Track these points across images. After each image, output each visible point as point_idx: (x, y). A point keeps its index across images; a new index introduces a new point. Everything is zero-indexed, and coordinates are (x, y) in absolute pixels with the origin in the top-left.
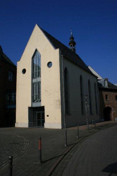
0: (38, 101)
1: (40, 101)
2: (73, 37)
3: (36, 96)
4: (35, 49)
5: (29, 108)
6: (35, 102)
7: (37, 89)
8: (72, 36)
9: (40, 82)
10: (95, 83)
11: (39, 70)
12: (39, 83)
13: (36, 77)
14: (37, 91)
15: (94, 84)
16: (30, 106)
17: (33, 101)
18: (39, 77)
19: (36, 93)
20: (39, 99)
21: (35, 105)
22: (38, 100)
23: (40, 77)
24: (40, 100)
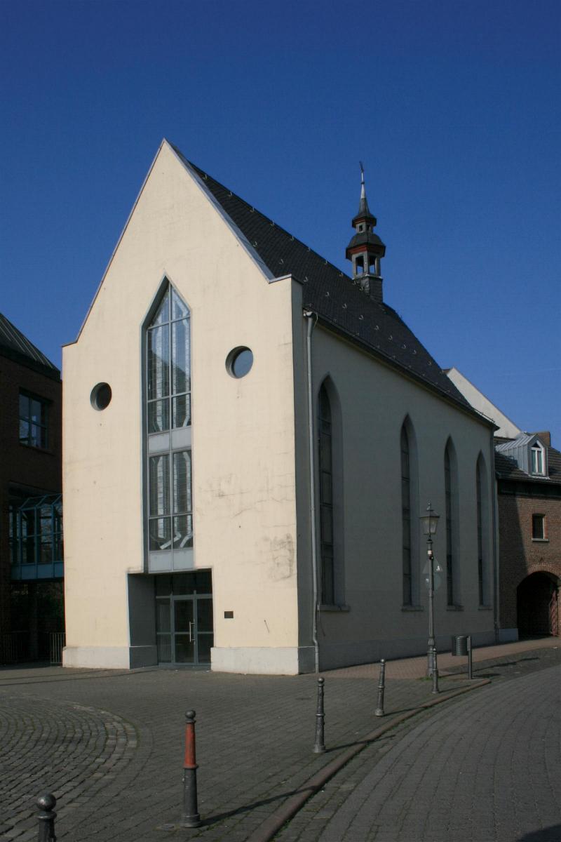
1: (190, 544)
4: (477, 453)
5: (133, 578)
7: (173, 483)
9: (189, 452)
10: (480, 455)
12: (183, 457)
14: (174, 494)
16: (138, 567)
17: (152, 543)
18: (180, 425)
19: (167, 510)
20: (184, 533)
21: (164, 563)
22: (176, 539)
23: (189, 423)
24: (187, 538)
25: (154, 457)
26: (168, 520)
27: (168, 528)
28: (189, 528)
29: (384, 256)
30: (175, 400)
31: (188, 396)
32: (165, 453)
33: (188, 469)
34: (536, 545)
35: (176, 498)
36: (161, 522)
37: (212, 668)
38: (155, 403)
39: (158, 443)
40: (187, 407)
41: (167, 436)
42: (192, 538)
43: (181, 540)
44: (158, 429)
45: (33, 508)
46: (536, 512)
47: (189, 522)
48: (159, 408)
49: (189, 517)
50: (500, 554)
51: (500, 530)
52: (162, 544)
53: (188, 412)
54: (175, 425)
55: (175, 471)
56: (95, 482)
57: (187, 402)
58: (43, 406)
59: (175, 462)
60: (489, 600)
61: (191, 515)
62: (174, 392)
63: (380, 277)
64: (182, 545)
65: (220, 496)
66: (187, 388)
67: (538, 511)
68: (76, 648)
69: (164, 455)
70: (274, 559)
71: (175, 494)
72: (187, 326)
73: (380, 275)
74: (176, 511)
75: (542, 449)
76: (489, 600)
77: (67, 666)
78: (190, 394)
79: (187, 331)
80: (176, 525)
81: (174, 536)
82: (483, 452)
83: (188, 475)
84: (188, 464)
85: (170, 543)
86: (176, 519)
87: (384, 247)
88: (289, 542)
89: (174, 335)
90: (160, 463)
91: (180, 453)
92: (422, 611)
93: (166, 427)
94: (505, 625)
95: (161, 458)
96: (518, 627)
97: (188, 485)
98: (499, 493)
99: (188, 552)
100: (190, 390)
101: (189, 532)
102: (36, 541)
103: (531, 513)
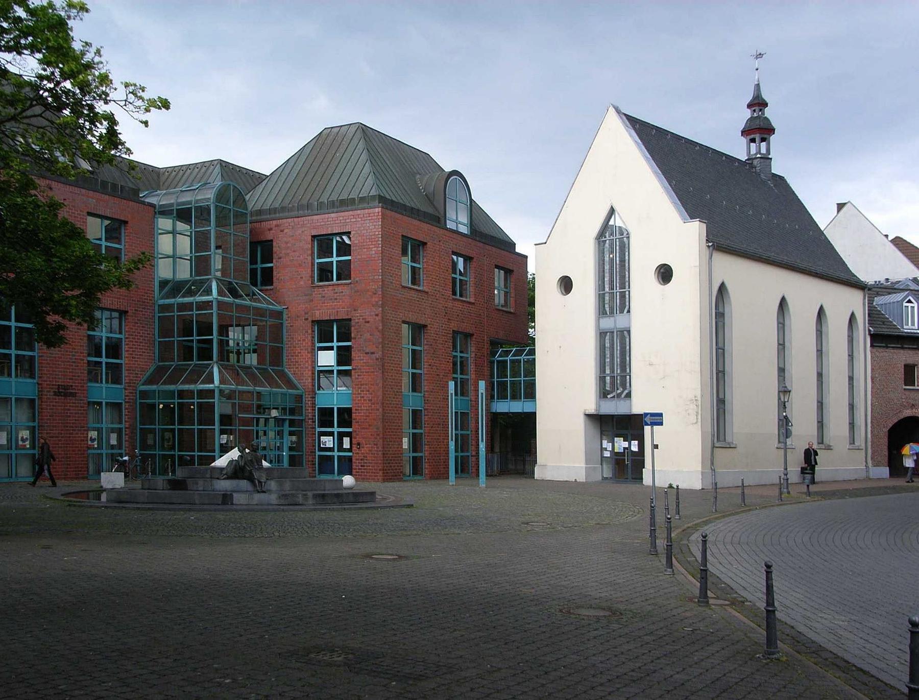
0: (619, 396)
1: (629, 395)
2: (765, 96)
3: (613, 378)
4: (851, 311)
5: (589, 416)
6: (609, 396)
7: (617, 353)
8: (758, 81)
9: (629, 332)
10: (852, 317)
11: (623, 286)
12: (624, 335)
13: (612, 312)
14: (617, 360)
15: (778, 302)
16: (592, 409)
17: (603, 394)
18: (622, 312)
19: (612, 370)
20: (624, 388)
21: (612, 407)
22: (619, 391)
23: (629, 311)
24: (626, 391)
25: (603, 333)
26: (613, 378)
27: (613, 383)
28: (628, 384)
29: (774, 134)
30: (618, 293)
31: (627, 293)
32: (612, 331)
33: (628, 343)
34: (907, 393)
35: (619, 363)
36: (608, 378)
37: (644, 483)
38: (604, 294)
39: (608, 323)
40: (627, 300)
41: (612, 319)
42: (630, 391)
43: (622, 392)
44: (607, 314)
45: (506, 358)
46: (907, 363)
47: (628, 380)
48: (607, 298)
49: (628, 377)
50: (872, 400)
51: (872, 379)
52: (608, 394)
53: (627, 304)
54: (618, 312)
55: (618, 344)
56: (560, 347)
57: (627, 296)
58: (505, 273)
59: (618, 337)
60: (860, 441)
61: (630, 376)
62: (618, 288)
63: (770, 157)
64: (623, 396)
65: (650, 365)
66: (627, 287)
67: (910, 361)
68: (546, 465)
69: (610, 332)
70: (686, 411)
71: (618, 360)
72: (627, 243)
73: (769, 154)
74: (619, 372)
75: (915, 305)
76: (860, 441)
77: (549, 477)
78: (629, 291)
79: (627, 246)
80: (618, 382)
81: (618, 389)
82: (856, 313)
83: (628, 348)
84: (628, 340)
85: (614, 394)
86: (618, 377)
87: (774, 130)
88: (696, 400)
89: (618, 248)
90: (607, 338)
91: (622, 332)
92: (831, 449)
93: (612, 312)
94: (877, 464)
95: (608, 334)
96: (889, 466)
97: (628, 354)
98: (872, 346)
99: (628, 401)
100: (629, 288)
101: (628, 387)
102: (263, 319)
103: (903, 364)
